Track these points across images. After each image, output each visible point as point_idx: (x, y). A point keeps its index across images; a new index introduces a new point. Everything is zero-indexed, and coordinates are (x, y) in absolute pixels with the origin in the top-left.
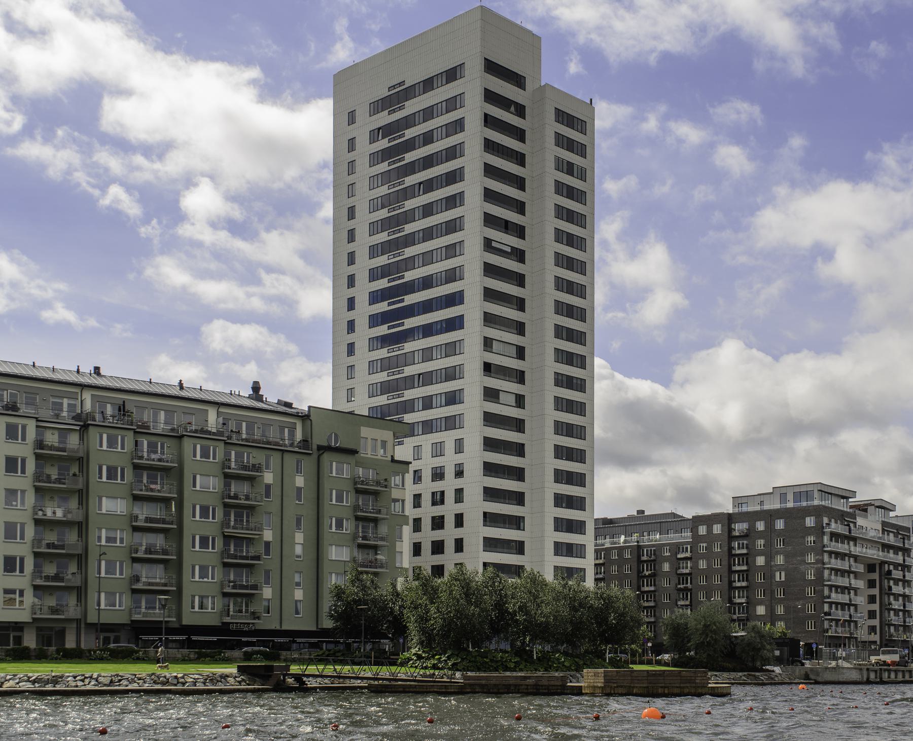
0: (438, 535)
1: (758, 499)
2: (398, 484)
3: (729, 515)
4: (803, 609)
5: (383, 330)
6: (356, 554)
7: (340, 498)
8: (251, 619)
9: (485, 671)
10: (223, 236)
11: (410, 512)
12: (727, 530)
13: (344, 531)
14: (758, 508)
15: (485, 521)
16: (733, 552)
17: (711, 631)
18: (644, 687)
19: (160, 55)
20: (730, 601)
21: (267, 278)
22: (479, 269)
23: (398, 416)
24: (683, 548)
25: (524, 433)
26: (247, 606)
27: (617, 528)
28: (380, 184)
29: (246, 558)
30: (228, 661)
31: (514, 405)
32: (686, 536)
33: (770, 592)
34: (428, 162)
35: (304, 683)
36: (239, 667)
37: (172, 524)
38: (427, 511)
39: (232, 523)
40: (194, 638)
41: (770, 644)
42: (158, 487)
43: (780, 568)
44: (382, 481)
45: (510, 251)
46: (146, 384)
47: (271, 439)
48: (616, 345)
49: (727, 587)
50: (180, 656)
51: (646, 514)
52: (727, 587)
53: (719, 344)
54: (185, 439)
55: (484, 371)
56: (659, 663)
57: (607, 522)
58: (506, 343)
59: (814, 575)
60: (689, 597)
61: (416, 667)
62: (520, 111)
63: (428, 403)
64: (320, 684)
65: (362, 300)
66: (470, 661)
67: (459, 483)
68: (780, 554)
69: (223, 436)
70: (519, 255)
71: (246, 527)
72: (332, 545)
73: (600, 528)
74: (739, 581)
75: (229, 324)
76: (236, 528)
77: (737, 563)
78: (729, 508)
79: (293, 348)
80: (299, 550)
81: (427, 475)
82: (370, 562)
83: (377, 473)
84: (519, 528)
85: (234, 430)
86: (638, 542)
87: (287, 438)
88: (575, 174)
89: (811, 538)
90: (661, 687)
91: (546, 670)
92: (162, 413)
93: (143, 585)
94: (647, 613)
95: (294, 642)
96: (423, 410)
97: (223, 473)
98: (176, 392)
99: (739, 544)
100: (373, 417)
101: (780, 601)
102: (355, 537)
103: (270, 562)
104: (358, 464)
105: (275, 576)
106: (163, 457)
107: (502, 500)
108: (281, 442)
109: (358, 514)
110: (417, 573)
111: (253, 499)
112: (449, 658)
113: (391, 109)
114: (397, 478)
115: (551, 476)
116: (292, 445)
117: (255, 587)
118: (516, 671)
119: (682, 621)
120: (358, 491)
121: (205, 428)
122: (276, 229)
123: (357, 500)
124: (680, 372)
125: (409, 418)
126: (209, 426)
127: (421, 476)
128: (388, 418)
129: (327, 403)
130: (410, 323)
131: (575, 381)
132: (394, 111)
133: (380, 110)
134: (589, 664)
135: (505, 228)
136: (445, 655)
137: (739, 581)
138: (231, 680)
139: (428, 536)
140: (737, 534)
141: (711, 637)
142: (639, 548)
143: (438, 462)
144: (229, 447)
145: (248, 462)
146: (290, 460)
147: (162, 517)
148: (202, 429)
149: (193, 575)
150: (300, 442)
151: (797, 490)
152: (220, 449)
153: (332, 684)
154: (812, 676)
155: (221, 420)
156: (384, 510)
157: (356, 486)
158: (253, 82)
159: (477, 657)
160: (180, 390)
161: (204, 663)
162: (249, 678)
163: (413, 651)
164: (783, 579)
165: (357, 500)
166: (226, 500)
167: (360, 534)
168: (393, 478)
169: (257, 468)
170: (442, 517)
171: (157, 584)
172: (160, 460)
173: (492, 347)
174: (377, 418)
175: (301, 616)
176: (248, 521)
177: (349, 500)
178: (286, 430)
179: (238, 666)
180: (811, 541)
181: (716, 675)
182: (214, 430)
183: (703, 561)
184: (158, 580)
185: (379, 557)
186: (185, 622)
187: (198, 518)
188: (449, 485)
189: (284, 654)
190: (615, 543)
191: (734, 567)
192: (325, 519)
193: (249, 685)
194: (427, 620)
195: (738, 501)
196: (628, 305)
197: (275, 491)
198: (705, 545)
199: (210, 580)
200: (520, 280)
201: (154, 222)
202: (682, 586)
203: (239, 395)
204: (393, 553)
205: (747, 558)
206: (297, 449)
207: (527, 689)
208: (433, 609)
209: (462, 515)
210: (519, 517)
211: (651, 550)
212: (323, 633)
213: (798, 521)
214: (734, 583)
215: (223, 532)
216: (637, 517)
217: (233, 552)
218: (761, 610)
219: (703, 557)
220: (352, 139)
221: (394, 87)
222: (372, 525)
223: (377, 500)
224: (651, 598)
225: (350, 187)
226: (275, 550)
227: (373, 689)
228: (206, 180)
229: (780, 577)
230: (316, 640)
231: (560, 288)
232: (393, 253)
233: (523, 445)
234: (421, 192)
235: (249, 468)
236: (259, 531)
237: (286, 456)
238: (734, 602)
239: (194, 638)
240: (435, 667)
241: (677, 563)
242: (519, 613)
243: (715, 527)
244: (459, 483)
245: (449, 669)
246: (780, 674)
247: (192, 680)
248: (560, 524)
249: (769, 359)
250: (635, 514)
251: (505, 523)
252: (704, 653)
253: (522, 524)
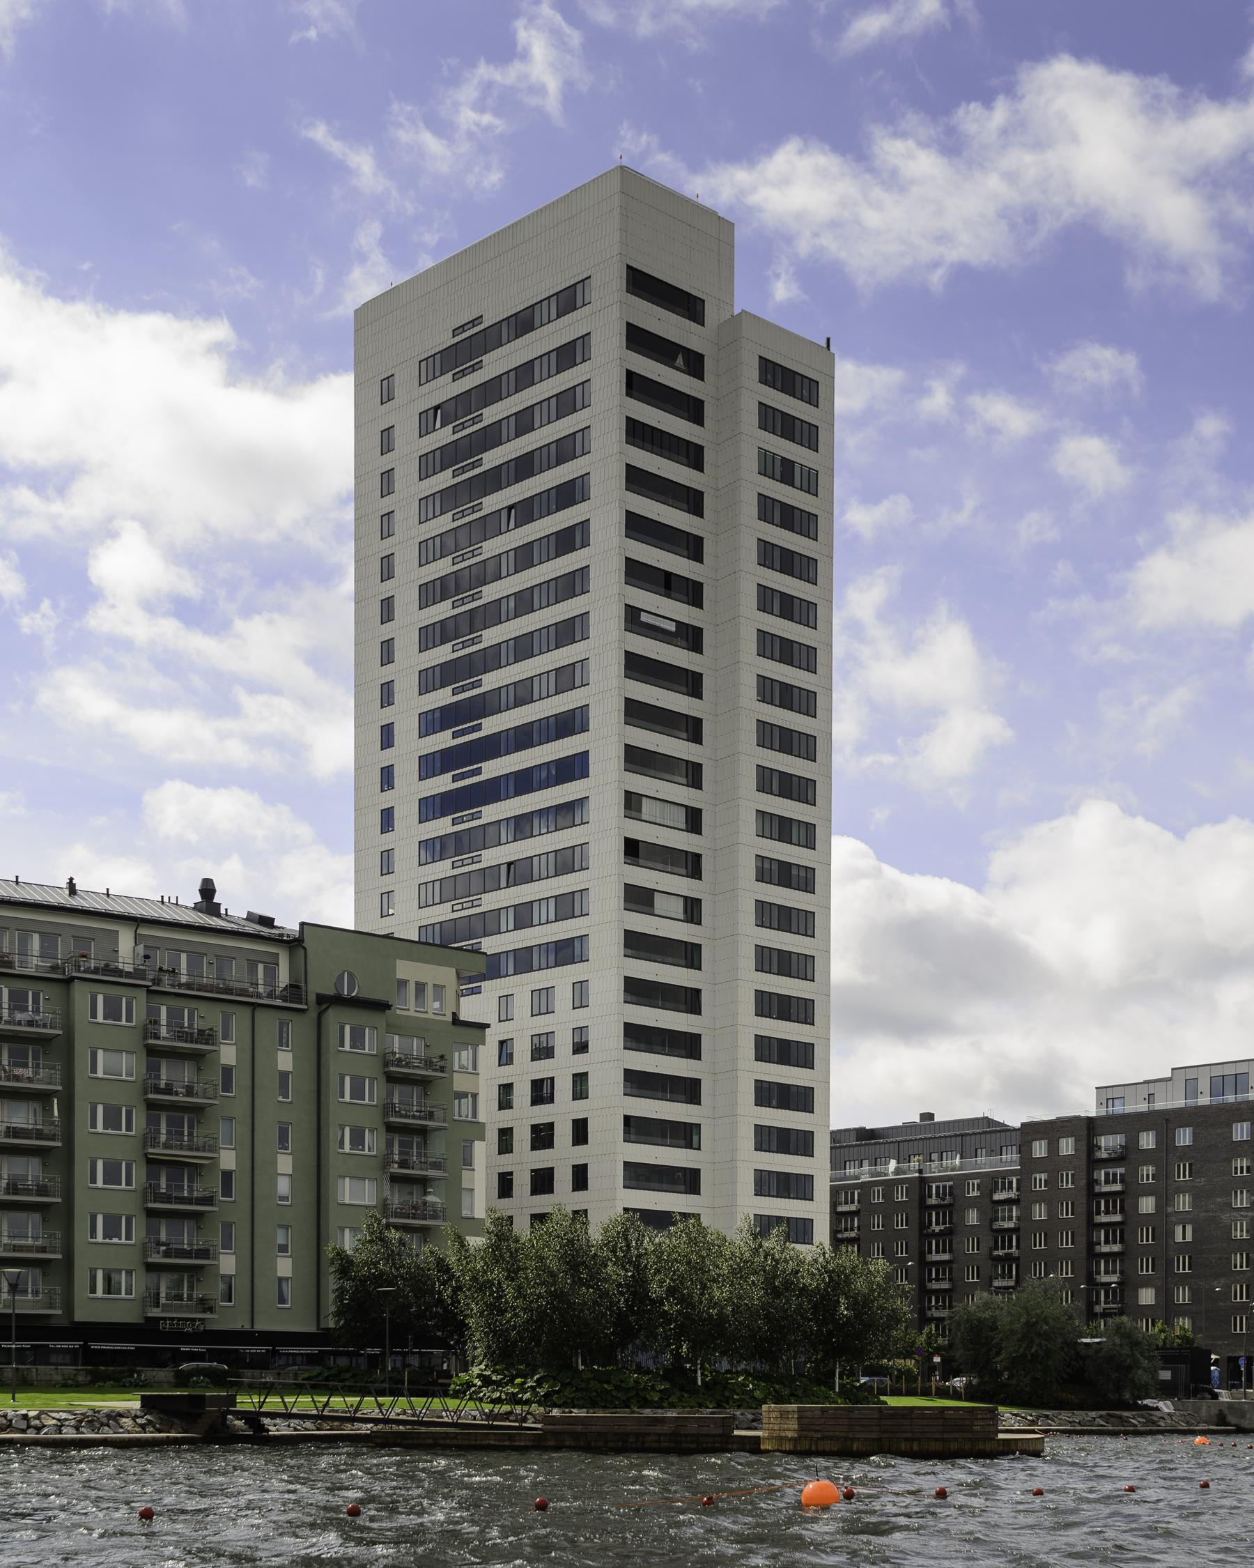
0: (542, 1159)
1: (1144, 1091)
2: (466, 1065)
3: (1090, 1120)
4: (1226, 1294)
5: (443, 783)
6: (387, 1192)
7: (357, 1092)
8: (196, 1312)
9: (605, 1407)
10: (169, 629)
11: (489, 1114)
12: (1085, 1148)
13: (367, 1152)
14: (1143, 1107)
15: (504, 1085)
16: (1097, 1189)
17: (1039, 1335)
18: (874, 1440)
19: (52, 304)
20: (1090, 1280)
21: (250, 703)
22: (616, 665)
23: (471, 942)
24: (1003, 1183)
25: (700, 969)
26: (191, 1288)
27: (882, 1146)
28: (438, 512)
29: (188, 1201)
30: (121, 1385)
31: (681, 917)
32: (1010, 1160)
33: (1164, 1262)
34: (524, 467)
35: (262, 1428)
36: (143, 1399)
37: (53, 1140)
38: (524, 1115)
39: (163, 1138)
40: (94, 1346)
41: (1150, 1358)
42: (29, 1072)
43: (1184, 1219)
44: (435, 1060)
45: (673, 629)
46: (9, 886)
47: (232, 984)
48: (880, 815)
49: (1084, 1254)
50: (59, 1378)
51: (937, 1119)
52: (1083, 1253)
53: (1074, 810)
54: (77, 983)
55: (625, 854)
56: (943, 1393)
57: (865, 1135)
58: (667, 801)
59: (1247, 1232)
60: (1014, 1273)
61: (481, 1400)
62: (694, 364)
63: (523, 916)
64: (296, 1429)
65: (406, 728)
66: (577, 1390)
67: (580, 1063)
68: (1184, 1192)
69: (144, 979)
70: (691, 637)
71: (188, 1146)
72: (343, 1177)
73: (852, 1146)
74: (1107, 1242)
75: (189, 788)
76: (170, 1147)
77: (1103, 1208)
78: (1090, 1108)
79: (304, 831)
80: (284, 1186)
81: (522, 1050)
82: (414, 1207)
83: (426, 1046)
84: (689, 1146)
85: (165, 968)
86: (920, 1171)
87: (261, 982)
88: (797, 482)
89: (1242, 1160)
90: (906, 1439)
91: (719, 1406)
92: (36, 937)
93: (4, 1250)
94: (937, 1302)
95: (275, 1352)
96: (515, 929)
97: (385, 1123)
98: (63, 899)
99: (1107, 1175)
100: (426, 944)
101: (1183, 1280)
102: (386, 1162)
103: (233, 1208)
104: (392, 1028)
105: (240, 1234)
106: (37, 1018)
107: (660, 1095)
108: (251, 990)
109: (392, 1119)
110: (502, 1230)
111: (200, 1094)
112: (539, 1383)
113: (457, 370)
114: (464, 1053)
115: (748, 1049)
116: (271, 995)
117: (204, 1253)
118: (662, 1408)
119: (987, 1315)
120: (391, 1079)
121: (113, 965)
122: (259, 613)
123: (390, 1094)
124: (1001, 863)
125: (490, 945)
126: (121, 960)
127: (512, 1054)
128: (452, 945)
129: (345, 919)
130: (492, 769)
131: (794, 872)
132: (463, 373)
133: (437, 374)
134: (800, 1395)
135: (665, 588)
136: (532, 1378)
137: (1107, 1242)
138: (126, 1422)
139: (524, 1160)
140: (1105, 1156)
141: (1040, 1345)
142: (923, 1182)
143: (542, 1024)
144: (157, 999)
145: (191, 1026)
146: (268, 1023)
147: (38, 1127)
148: (107, 965)
149: (93, 1233)
150: (285, 989)
151: (1218, 1072)
152: (140, 1002)
153: (318, 1430)
154: (1232, 1419)
155: (141, 949)
156: (438, 1113)
157: (386, 1070)
158: (216, 348)
159: (591, 1381)
160: (70, 895)
161: (102, 1391)
162: (161, 1419)
163: (476, 1370)
164: (1189, 1238)
165: (390, 1094)
166: (151, 1096)
167: (396, 1158)
168: (457, 1054)
169: (206, 1036)
170: (551, 1126)
171: (28, 1249)
172: (30, 1023)
173: (640, 811)
174: (433, 945)
175: (289, 1306)
176: (190, 1134)
177: (374, 1094)
178: (261, 967)
179: (142, 1396)
180: (1242, 1168)
181: (1047, 1417)
182: (129, 968)
183: (1040, 1205)
184: (30, 1242)
185: (429, 1198)
186: (80, 1316)
187: (100, 1128)
188: (561, 1068)
189: (248, 1376)
190: (879, 1174)
191: (1099, 1217)
192: (331, 1130)
193: (160, 1431)
194: (502, 1312)
195: (1106, 1094)
196: (900, 741)
197: (240, 1080)
198: (1043, 1176)
199: (123, 1241)
200: (692, 684)
201: (46, 605)
202: (1001, 1253)
203: (177, 904)
204: (456, 1191)
205: (1124, 1201)
206: (279, 1002)
207: (659, 1441)
208: (510, 1292)
209: (585, 1121)
210: (691, 1124)
211: (944, 1187)
212: (320, 1337)
213: (1219, 1131)
214: (1098, 1247)
215: (146, 1155)
216: (920, 1126)
217: (164, 1191)
218: (1147, 1296)
219: (1040, 1198)
220: (388, 429)
221: (462, 328)
222: (416, 1139)
223: (426, 1094)
224: (944, 1274)
225: (385, 518)
226: (240, 1186)
227: (379, 1441)
228: (135, 525)
229: (1183, 1234)
230: (315, 1350)
231: (768, 698)
232: (461, 640)
233: (698, 991)
234: (512, 525)
235: (192, 1038)
236: (210, 1151)
237: (261, 1015)
238: (1098, 1281)
239: (94, 1346)
240: (513, 1399)
241: (991, 1208)
242: (666, 1299)
243: (1063, 1142)
244: (580, 1063)
245: (540, 1404)
246: (1169, 1414)
247: (54, 1422)
248: (765, 1138)
249: (1168, 836)
250: (918, 1120)
251: (664, 1136)
252: (1025, 1376)
253: (695, 1138)
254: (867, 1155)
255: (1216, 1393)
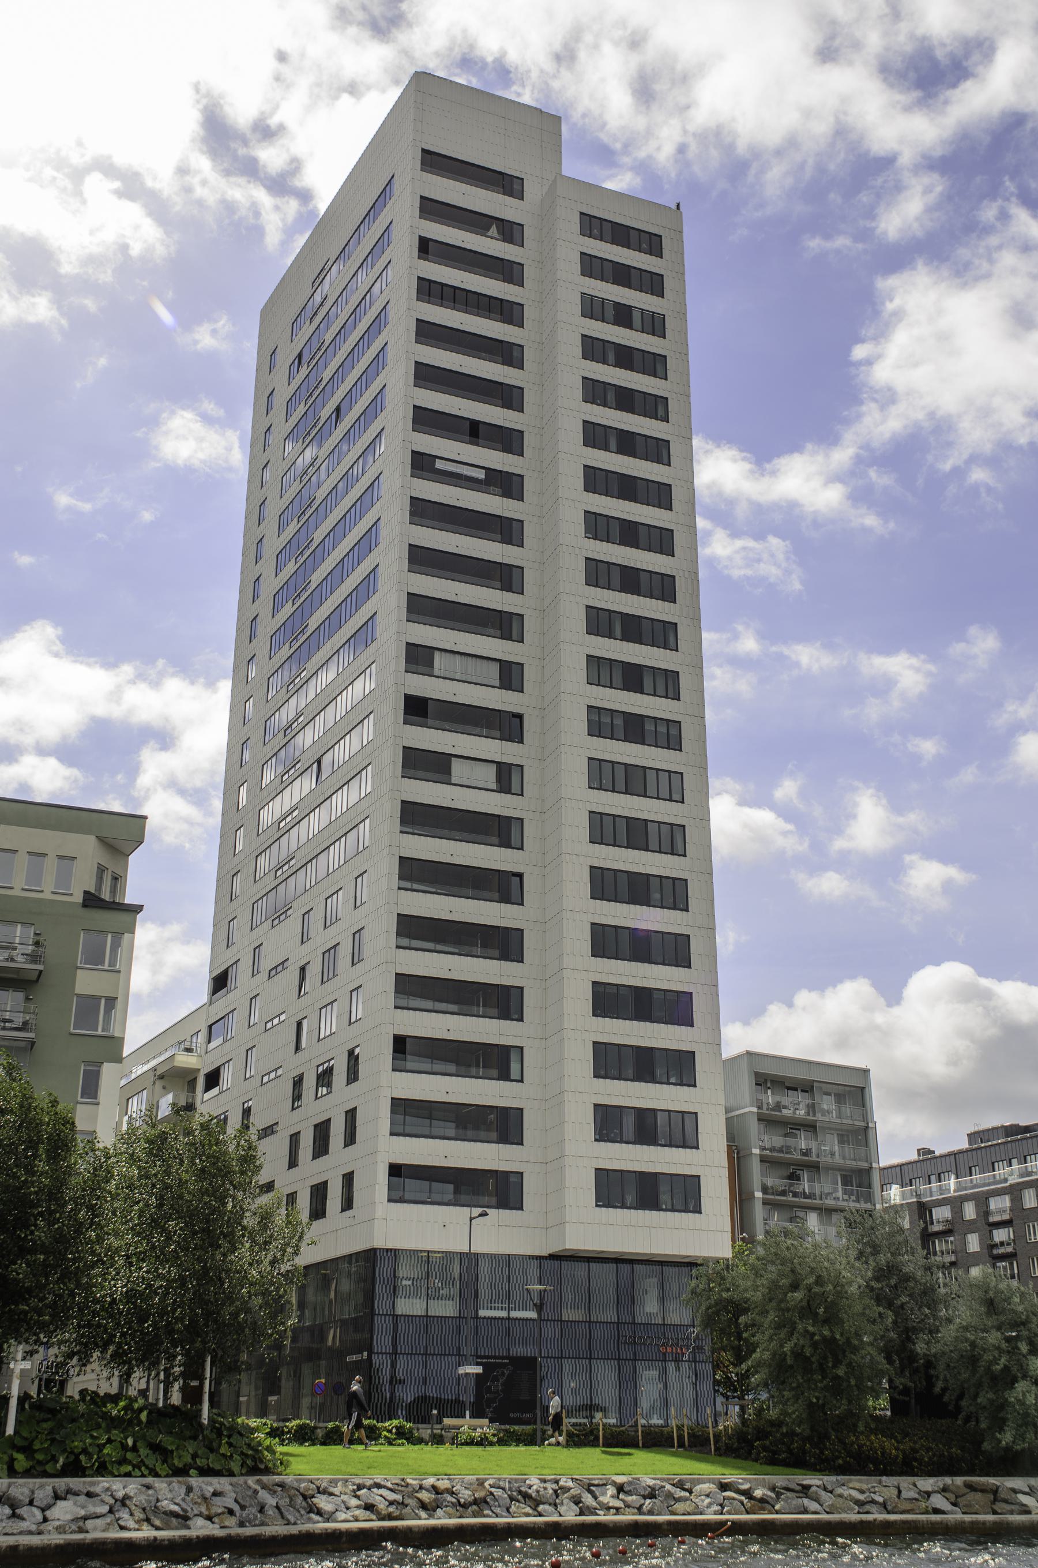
31: (494, 786)
84: (504, 1075)
135: (471, 435)
181: (805, 1489)
254: (1015, 1153)
255: (465, 1414)
